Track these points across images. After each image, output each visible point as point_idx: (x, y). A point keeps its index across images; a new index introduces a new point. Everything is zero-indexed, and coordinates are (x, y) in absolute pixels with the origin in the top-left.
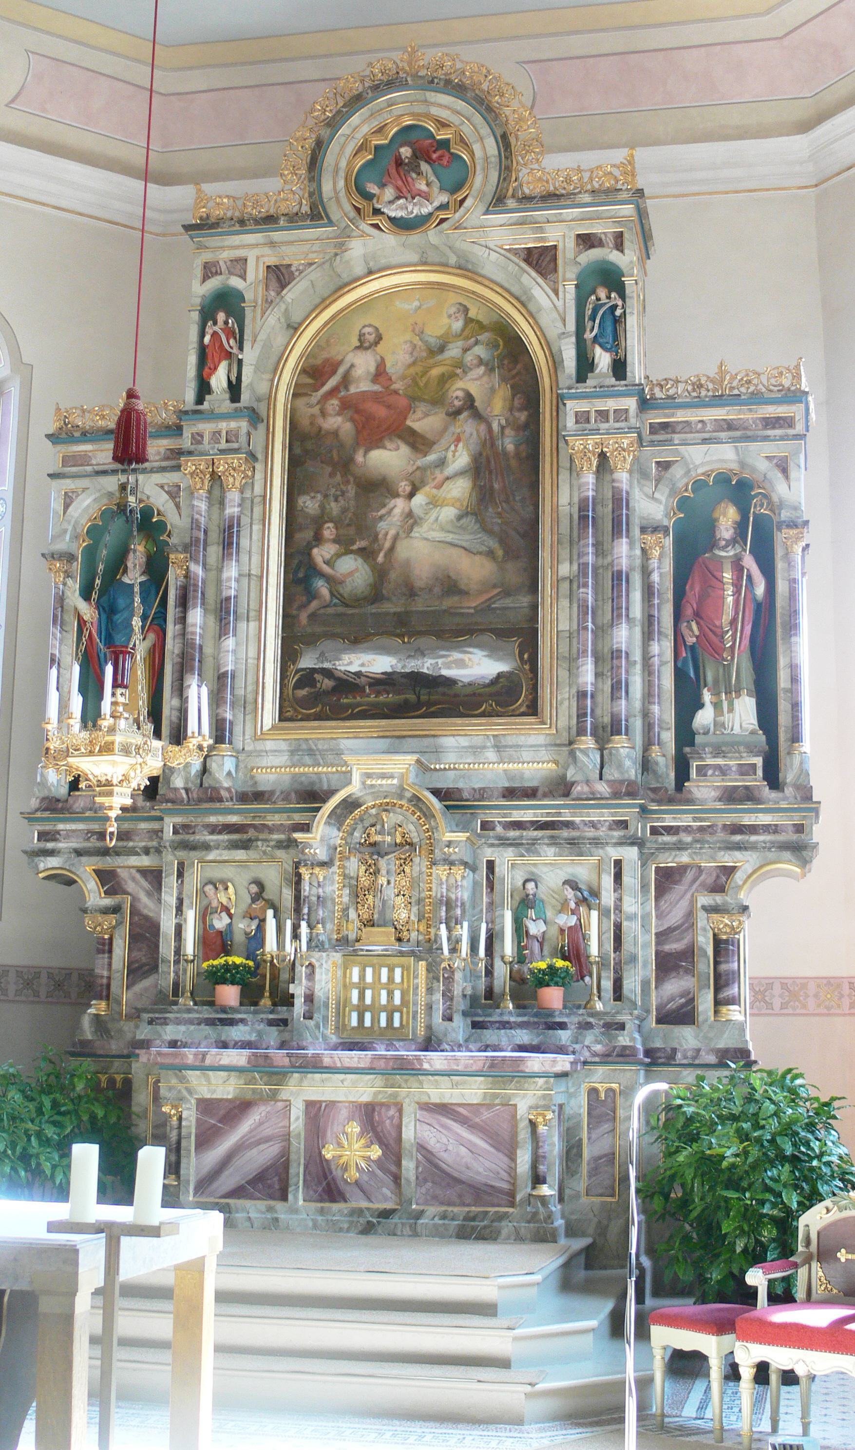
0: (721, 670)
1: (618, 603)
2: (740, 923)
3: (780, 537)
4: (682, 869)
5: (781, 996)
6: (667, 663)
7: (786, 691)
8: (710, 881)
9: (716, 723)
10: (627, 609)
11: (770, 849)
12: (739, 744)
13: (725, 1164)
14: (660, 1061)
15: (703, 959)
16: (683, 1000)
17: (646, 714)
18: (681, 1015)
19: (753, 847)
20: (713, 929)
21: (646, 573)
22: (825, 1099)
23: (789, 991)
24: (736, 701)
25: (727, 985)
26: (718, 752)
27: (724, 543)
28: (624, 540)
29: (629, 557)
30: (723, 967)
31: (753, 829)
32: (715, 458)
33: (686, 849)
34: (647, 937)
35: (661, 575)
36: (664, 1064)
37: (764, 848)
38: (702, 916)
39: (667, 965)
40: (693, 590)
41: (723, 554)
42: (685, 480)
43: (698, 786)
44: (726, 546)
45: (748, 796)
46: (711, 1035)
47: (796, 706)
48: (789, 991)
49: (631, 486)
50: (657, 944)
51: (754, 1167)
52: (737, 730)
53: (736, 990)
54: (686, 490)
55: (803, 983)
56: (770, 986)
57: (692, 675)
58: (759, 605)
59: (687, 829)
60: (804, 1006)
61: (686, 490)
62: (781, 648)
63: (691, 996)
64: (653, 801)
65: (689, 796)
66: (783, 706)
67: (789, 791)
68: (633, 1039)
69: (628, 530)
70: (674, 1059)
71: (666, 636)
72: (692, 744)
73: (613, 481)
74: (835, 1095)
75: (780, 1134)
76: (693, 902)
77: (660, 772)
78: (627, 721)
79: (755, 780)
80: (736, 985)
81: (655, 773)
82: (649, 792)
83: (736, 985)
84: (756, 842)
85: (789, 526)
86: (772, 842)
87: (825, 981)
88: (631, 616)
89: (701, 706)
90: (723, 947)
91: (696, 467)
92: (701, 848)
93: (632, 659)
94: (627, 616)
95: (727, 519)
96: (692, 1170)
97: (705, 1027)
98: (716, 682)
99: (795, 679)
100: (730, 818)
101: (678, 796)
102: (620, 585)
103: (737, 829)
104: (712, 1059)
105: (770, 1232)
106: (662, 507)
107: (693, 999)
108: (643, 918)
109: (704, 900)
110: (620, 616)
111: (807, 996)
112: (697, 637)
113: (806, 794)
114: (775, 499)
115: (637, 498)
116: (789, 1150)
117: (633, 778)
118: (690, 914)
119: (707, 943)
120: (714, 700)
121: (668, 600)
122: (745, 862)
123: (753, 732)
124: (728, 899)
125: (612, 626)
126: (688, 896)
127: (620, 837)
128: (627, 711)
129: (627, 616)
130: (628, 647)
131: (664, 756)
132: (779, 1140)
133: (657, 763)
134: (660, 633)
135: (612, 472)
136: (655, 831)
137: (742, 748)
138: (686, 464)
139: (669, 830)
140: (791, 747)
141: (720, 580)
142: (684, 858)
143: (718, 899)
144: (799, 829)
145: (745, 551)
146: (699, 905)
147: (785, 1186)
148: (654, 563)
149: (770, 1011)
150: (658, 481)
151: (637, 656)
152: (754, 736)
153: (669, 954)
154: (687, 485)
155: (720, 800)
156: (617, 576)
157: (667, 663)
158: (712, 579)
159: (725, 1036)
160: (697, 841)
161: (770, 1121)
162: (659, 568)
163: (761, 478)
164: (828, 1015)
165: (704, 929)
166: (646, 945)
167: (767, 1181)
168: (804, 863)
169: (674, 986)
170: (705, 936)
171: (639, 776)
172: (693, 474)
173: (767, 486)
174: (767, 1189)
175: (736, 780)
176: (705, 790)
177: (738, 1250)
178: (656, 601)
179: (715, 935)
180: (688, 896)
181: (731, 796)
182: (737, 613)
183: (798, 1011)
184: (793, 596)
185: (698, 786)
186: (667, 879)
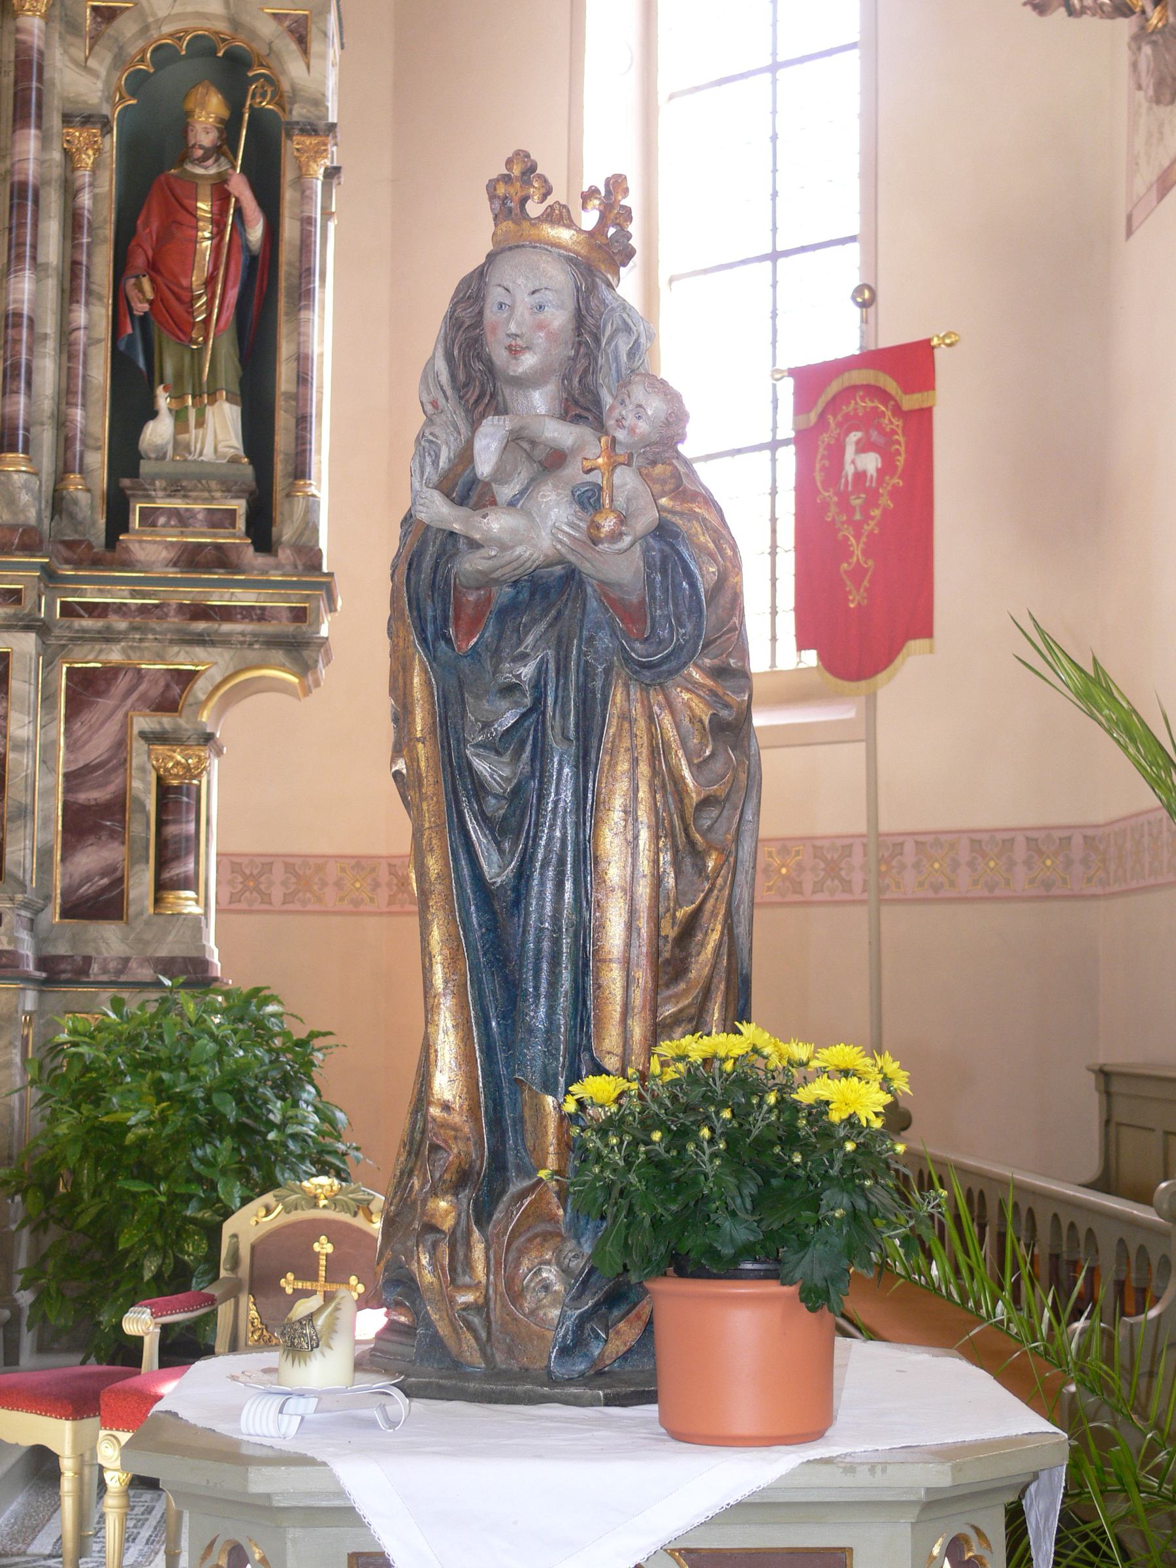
0: (187, 359)
1: (18, 237)
2: (200, 760)
3: (292, 147)
4: (110, 673)
5: (283, 883)
6: (99, 341)
7: (290, 396)
8: (155, 692)
9: (176, 444)
10: (34, 247)
11: (251, 644)
12: (209, 477)
13: (130, 1137)
14: (64, 976)
15: (139, 816)
16: (105, 881)
17: (61, 423)
18: (100, 904)
19: (224, 641)
20: (157, 770)
21: (70, 191)
22: (300, 1033)
23: (297, 875)
24: (209, 411)
25: (177, 857)
26: (176, 488)
27: (200, 153)
28: (33, 131)
29: (41, 162)
30: (171, 830)
31: (227, 613)
32: (189, 9)
33: (118, 641)
34: (50, 779)
35: (95, 198)
36: (68, 982)
37: (242, 643)
38: (139, 748)
39: (81, 824)
40: (149, 228)
41: (199, 171)
42: (141, 44)
43: (140, 542)
44: (204, 158)
45: (220, 560)
46: (148, 936)
47: (302, 422)
48: (297, 875)
49: (48, 43)
50: (67, 790)
51: (176, 1142)
52: (208, 454)
53: (192, 866)
54: (142, 60)
55: (320, 863)
56: (267, 867)
57: (141, 363)
58: (253, 260)
59: (121, 609)
60: (319, 900)
61: (142, 60)
62: (284, 329)
63: (118, 874)
64: (67, 561)
65: (125, 556)
66: (283, 420)
67: (285, 555)
68: (14, 940)
69: (39, 117)
70: (87, 974)
71: (100, 298)
72: (134, 473)
73: (18, 30)
74: (316, 1029)
75: (220, 1089)
76: (126, 725)
77: (80, 516)
78: (27, 429)
79: (234, 536)
80: (192, 859)
81: (72, 516)
82: (61, 548)
83: (192, 859)
84: (230, 634)
85: (304, 131)
86: (254, 635)
87: (353, 862)
88: (41, 259)
89: (153, 414)
90: (174, 798)
91: (159, 22)
92: (141, 640)
93: (40, 330)
94: (34, 258)
95: (207, 113)
96: (78, 1148)
97: (139, 925)
98: (179, 376)
99: (303, 379)
100: (188, 595)
101: (109, 555)
102: (22, 207)
103: (201, 612)
104: (147, 974)
105: (197, 1247)
106: (100, 85)
107: (120, 880)
108: (44, 748)
109: (143, 722)
110: (20, 257)
111: (324, 884)
112: (151, 303)
113: (310, 559)
114: (286, 86)
115: (59, 64)
116: (231, 1112)
117: (33, 521)
118: (121, 745)
119: (147, 791)
120: (174, 406)
121: (105, 241)
122: (210, 664)
123: (234, 460)
124: (182, 722)
125: (8, 274)
126: (119, 715)
127: (7, 617)
128: (28, 413)
129: (34, 258)
130: (32, 309)
131: (88, 490)
132: (216, 1099)
133: (75, 502)
134: (89, 292)
135: (15, 15)
136: (68, 610)
137: (213, 484)
138: (142, 15)
139: (93, 610)
140: (292, 484)
141: (192, 213)
142: (115, 655)
143: (167, 721)
144: (299, 615)
145: (234, 167)
146: (136, 731)
147: (224, 1172)
148: (84, 176)
149: (268, 907)
150: (95, 39)
151: (49, 325)
152: (235, 466)
153: (86, 808)
154: (144, 51)
155: (175, 565)
156: (19, 192)
157: (99, 341)
158: (179, 214)
159: (171, 938)
160: (134, 629)
161: (205, 1068)
162: (91, 185)
163: (264, 51)
164: (352, 913)
165: (143, 769)
166: (48, 792)
167: (195, 1165)
168: (304, 668)
169: (92, 859)
170: (143, 780)
171: (46, 522)
172: (155, 34)
173: (273, 63)
174: (200, 1179)
175: (203, 535)
176: (150, 547)
177: (147, 1276)
178: (85, 240)
179: (160, 779)
180: (119, 715)
181: (193, 559)
182: (216, 268)
183: (309, 907)
184: (305, 246)
185: (140, 542)
186: (86, 687)
